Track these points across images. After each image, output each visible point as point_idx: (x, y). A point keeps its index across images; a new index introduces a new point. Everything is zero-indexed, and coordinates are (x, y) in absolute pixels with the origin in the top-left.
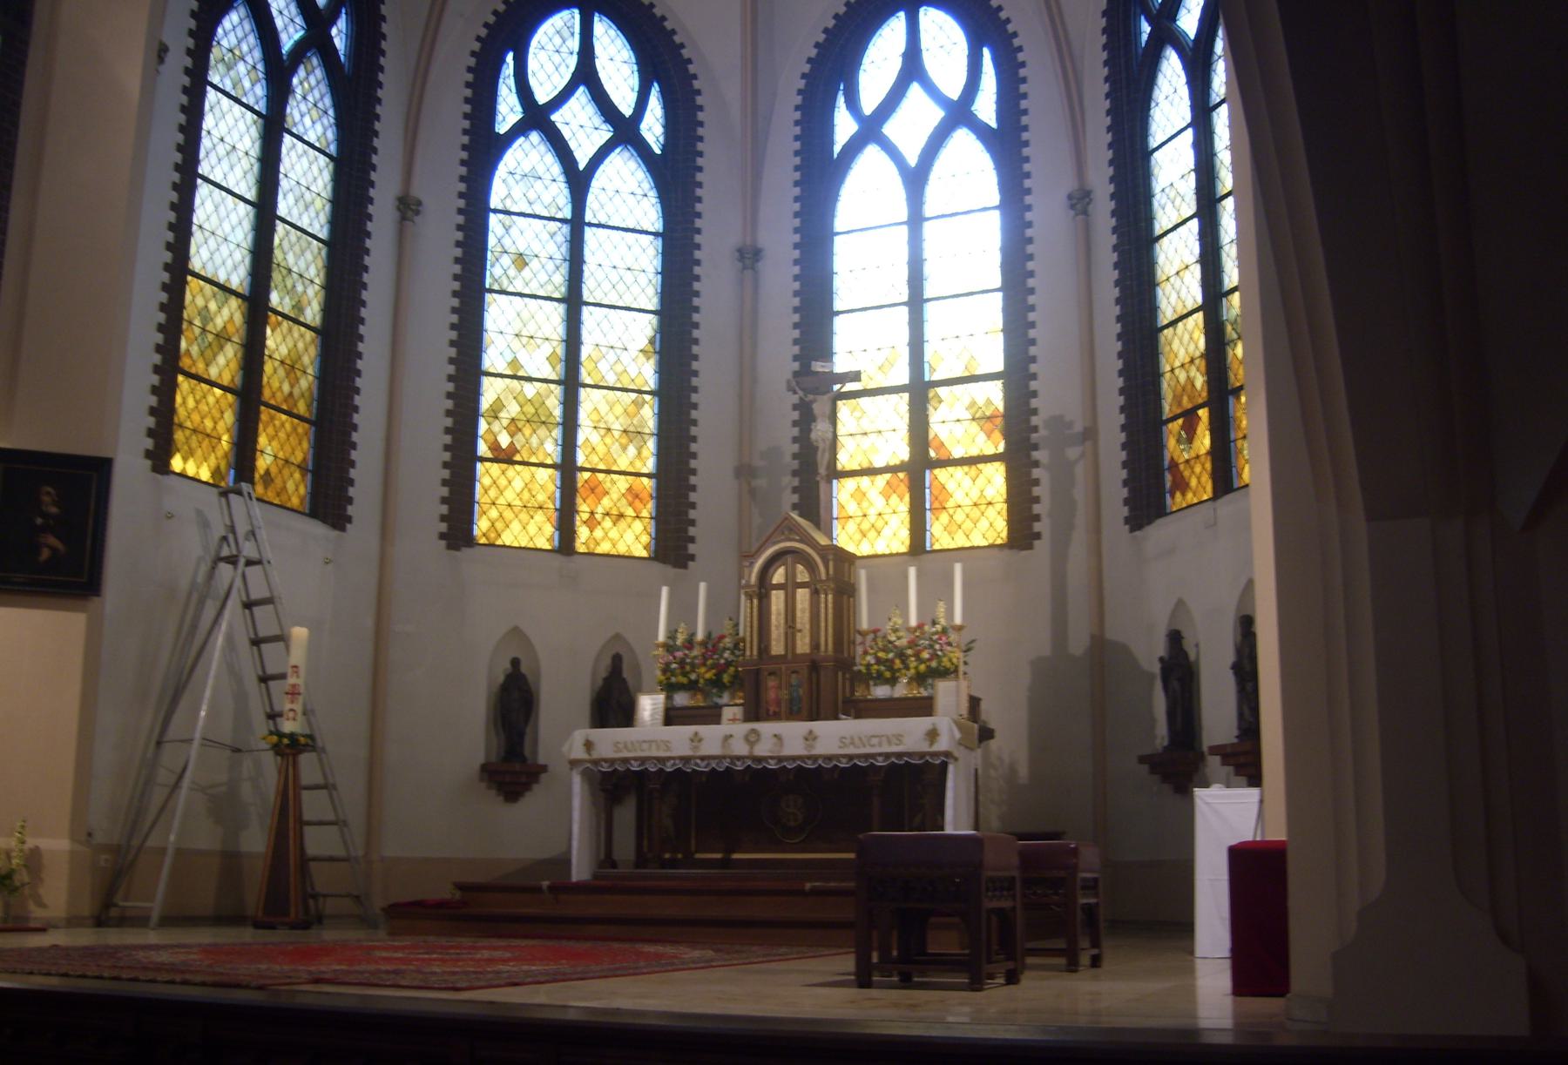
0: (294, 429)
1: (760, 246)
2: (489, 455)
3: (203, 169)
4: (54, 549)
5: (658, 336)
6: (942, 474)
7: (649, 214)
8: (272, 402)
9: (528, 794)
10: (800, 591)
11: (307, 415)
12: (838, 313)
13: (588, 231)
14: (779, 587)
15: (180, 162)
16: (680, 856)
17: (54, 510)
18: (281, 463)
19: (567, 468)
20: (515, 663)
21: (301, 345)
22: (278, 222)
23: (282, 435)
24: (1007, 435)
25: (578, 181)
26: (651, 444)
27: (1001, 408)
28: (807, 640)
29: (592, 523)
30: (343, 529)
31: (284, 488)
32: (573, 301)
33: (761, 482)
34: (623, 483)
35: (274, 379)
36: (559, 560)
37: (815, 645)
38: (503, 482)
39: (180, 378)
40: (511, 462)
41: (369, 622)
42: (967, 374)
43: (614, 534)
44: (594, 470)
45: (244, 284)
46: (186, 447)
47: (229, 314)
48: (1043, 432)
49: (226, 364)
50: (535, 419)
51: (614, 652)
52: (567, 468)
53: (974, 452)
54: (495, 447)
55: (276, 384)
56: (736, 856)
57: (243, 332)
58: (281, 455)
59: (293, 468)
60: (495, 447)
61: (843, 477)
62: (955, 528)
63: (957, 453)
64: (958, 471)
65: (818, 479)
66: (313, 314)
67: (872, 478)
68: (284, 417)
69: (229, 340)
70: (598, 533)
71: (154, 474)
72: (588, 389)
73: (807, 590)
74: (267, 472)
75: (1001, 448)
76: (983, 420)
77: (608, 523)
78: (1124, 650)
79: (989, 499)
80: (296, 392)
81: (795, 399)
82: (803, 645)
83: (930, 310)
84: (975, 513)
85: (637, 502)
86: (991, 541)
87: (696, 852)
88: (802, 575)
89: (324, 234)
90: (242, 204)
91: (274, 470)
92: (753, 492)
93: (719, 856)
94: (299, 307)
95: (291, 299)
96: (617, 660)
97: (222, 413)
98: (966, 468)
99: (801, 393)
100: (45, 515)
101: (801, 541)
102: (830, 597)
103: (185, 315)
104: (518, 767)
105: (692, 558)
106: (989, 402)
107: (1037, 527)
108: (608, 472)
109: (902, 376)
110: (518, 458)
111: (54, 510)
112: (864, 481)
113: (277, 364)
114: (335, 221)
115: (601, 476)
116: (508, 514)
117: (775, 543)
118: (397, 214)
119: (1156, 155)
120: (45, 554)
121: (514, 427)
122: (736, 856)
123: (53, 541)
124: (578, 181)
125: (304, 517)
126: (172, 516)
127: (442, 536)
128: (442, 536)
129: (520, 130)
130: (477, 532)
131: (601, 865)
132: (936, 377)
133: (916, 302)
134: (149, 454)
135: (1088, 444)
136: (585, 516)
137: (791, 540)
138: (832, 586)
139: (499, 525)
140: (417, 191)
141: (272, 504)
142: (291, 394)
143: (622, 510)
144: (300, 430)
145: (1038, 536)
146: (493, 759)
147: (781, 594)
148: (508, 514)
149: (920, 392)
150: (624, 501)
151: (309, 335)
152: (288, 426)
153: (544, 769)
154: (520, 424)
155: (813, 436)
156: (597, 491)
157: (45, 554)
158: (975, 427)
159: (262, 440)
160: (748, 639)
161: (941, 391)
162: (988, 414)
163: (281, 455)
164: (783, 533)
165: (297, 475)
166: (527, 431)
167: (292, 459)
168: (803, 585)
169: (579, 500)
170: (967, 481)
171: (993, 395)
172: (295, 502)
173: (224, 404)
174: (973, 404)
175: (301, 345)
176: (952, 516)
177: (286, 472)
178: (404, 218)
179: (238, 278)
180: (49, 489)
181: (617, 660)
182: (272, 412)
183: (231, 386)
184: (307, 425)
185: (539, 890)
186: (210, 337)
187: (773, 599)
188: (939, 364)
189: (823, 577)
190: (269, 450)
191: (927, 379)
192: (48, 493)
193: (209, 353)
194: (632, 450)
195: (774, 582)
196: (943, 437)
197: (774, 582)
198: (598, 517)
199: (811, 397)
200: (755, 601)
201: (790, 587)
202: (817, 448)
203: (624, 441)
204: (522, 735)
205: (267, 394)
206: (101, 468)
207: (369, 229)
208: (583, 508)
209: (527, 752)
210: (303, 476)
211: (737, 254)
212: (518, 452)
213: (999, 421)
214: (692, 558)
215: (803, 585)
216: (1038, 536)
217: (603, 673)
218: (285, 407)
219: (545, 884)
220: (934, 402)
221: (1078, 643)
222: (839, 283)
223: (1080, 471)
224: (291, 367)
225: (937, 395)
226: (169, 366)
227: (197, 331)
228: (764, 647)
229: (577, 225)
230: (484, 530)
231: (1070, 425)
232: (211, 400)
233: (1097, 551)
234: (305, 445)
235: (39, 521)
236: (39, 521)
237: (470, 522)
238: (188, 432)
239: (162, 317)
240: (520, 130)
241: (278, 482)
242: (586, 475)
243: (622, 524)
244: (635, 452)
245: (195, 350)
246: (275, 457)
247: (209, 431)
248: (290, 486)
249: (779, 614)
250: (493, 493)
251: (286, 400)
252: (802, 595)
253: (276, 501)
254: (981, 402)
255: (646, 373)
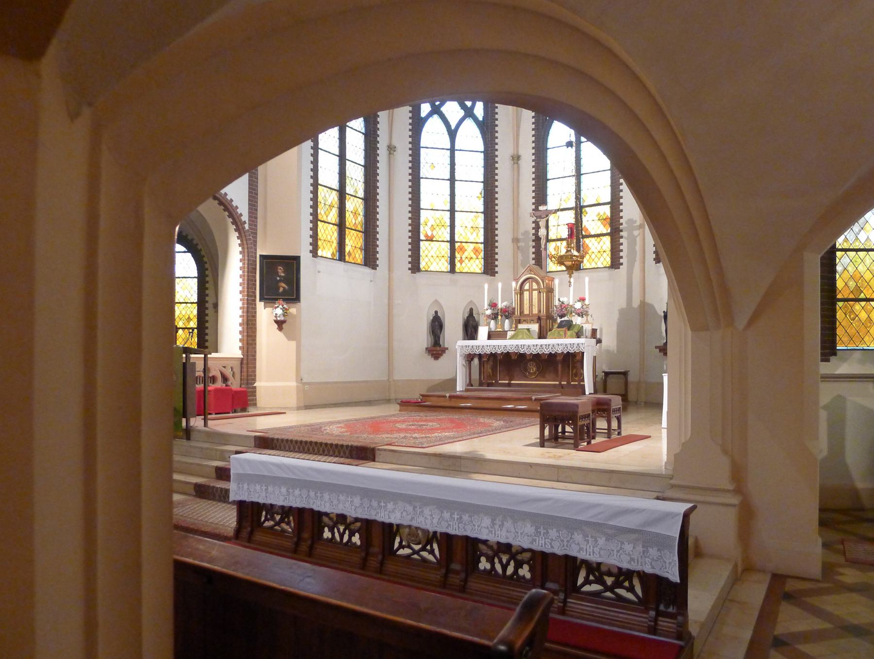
0: (357, 235)
1: (520, 154)
2: (424, 239)
3: (320, 146)
4: (284, 288)
5: (483, 191)
6: (587, 240)
7: (480, 145)
8: (349, 227)
9: (441, 357)
10: (534, 292)
11: (361, 230)
12: (549, 180)
13: (456, 152)
14: (527, 290)
15: (312, 175)
16: (494, 382)
17: (283, 274)
18: (353, 248)
19: (452, 242)
20: (436, 312)
21: (357, 205)
22: (347, 161)
23: (353, 238)
24: (611, 225)
25: (452, 134)
26: (482, 231)
27: (609, 216)
28: (537, 309)
29: (461, 261)
30: (376, 269)
31: (355, 257)
32: (452, 180)
33: (521, 244)
34: (472, 246)
35: (350, 219)
36: (450, 276)
37: (540, 311)
38: (429, 248)
39: (319, 222)
40: (432, 240)
41: (386, 301)
42: (597, 203)
43: (469, 265)
44: (461, 242)
45: (337, 220)
46: (322, 247)
47: (334, 197)
48: (624, 225)
49: (333, 216)
50: (440, 224)
51: (470, 307)
52: (452, 242)
53: (599, 232)
54: (426, 236)
55: (350, 220)
56: (512, 382)
57: (338, 203)
58: (353, 245)
59: (358, 249)
60: (426, 236)
61: (551, 242)
62: (591, 260)
63: (593, 233)
64: (593, 239)
65: (541, 249)
66: (361, 194)
67: (561, 242)
68: (354, 231)
69: (334, 207)
70: (463, 264)
71: (313, 258)
72: (458, 212)
73: (537, 291)
74: (349, 252)
75: (609, 231)
76: (603, 220)
77: (467, 261)
78: (651, 307)
79: (604, 250)
80: (357, 222)
81: (534, 219)
82: (535, 311)
83: (583, 178)
84: (599, 255)
85: (477, 253)
86: (605, 265)
87: (499, 380)
88: (535, 286)
89: (363, 163)
90: (334, 191)
91: (351, 251)
92: (518, 248)
93: (507, 382)
94: (356, 191)
95: (353, 189)
96: (471, 310)
97: (333, 233)
98: (596, 238)
99: (535, 218)
100: (280, 276)
101: (534, 274)
102: (545, 294)
103: (319, 201)
104: (438, 348)
105: (497, 272)
106: (605, 213)
107: (621, 261)
108: (466, 242)
109: (572, 204)
110: (434, 239)
111: (283, 274)
112: (559, 243)
113: (350, 213)
114: (367, 157)
115: (464, 244)
116: (432, 259)
117: (525, 275)
118: (388, 152)
119: (646, 301)
120: (281, 290)
121: (433, 228)
122: (512, 382)
123: (283, 285)
124: (452, 134)
125: (362, 266)
126: (320, 272)
127: (409, 269)
128: (409, 269)
129: (430, 115)
130: (421, 266)
131: (468, 385)
132: (585, 204)
133: (578, 175)
134: (311, 252)
135: (641, 230)
136: (459, 259)
137: (530, 274)
138: (545, 290)
139: (429, 264)
140: (395, 143)
141: (351, 263)
142: (355, 223)
143: (472, 256)
144: (359, 235)
145: (622, 264)
146: (429, 346)
147: (528, 292)
148: (432, 259)
149: (579, 210)
150: (472, 253)
151: (360, 201)
152: (355, 235)
153: (447, 349)
154: (435, 227)
155: (539, 234)
156: (462, 250)
157: (281, 290)
158: (599, 223)
159: (347, 241)
160: (516, 308)
161: (587, 209)
162: (604, 218)
163: (353, 245)
164: (528, 272)
165: (359, 251)
166: (437, 229)
167: (357, 246)
168: (535, 290)
169: (456, 253)
170: (596, 243)
171: (606, 210)
172: (359, 261)
173: (333, 230)
174: (599, 214)
175: (357, 205)
176: (590, 256)
177: (355, 251)
178: (390, 154)
179: (335, 184)
180: (280, 267)
181: (471, 310)
182: (350, 230)
183: (335, 223)
184: (361, 233)
185: (445, 397)
186: (327, 206)
187: (525, 295)
188: (587, 199)
189: (542, 287)
190: (349, 244)
191: (582, 205)
192: (280, 269)
193: (327, 213)
194: (475, 234)
195: (525, 288)
196: (588, 227)
197: (525, 288)
198: (463, 259)
199: (538, 220)
200: (519, 295)
201: (531, 290)
202: (541, 238)
203: (472, 230)
204: (439, 338)
205: (347, 224)
206: (297, 259)
207: (378, 172)
208: (458, 255)
209: (441, 343)
210: (361, 252)
211: (511, 158)
212: (434, 237)
213: (608, 220)
214: (497, 272)
215: (535, 290)
216: (622, 264)
217: (466, 315)
218: (353, 228)
219: (448, 395)
220: (584, 214)
221: (636, 303)
222: (549, 168)
223: (638, 239)
224: (355, 214)
225: (585, 211)
226: (315, 219)
227: (323, 205)
228: (522, 312)
229: (452, 150)
230: (424, 265)
231: (635, 222)
232: (329, 229)
233: (643, 270)
234: (361, 240)
235: (278, 278)
236: (278, 278)
237: (419, 263)
238: (322, 241)
239: (311, 225)
240: (430, 115)
241: (353, 255)
242: (459, 244)
243: (472, 261)
244: (476, 235)
245: (323, 212)
246: (352, 246)
247: (329, 240)
248: (357, 256)
249: (527, 300)
250: (426, 252)
251: (354, 226)
252: (535, 293)
253: (353, 262)
254: (602, 213)
255: (480, 206)
